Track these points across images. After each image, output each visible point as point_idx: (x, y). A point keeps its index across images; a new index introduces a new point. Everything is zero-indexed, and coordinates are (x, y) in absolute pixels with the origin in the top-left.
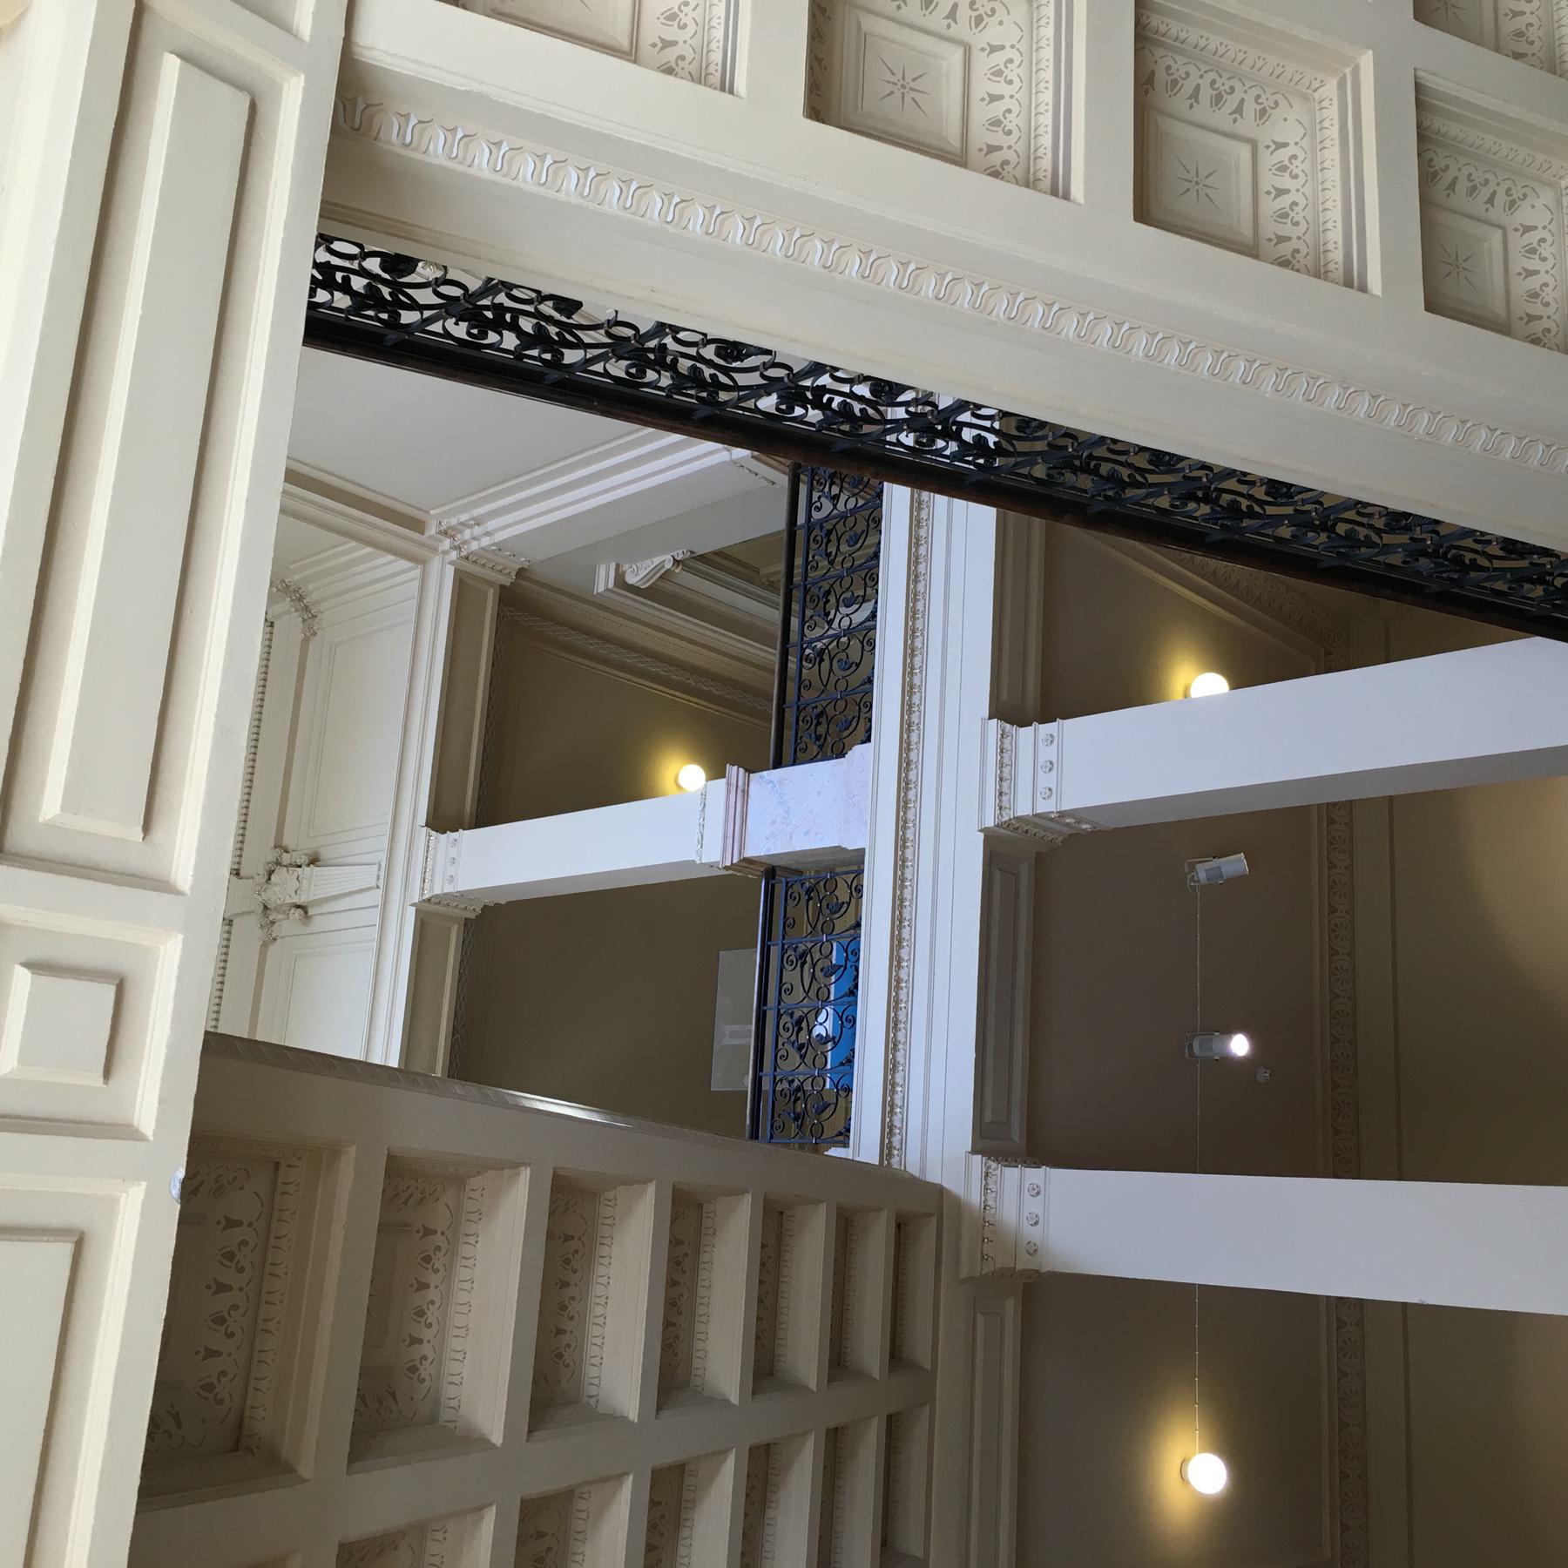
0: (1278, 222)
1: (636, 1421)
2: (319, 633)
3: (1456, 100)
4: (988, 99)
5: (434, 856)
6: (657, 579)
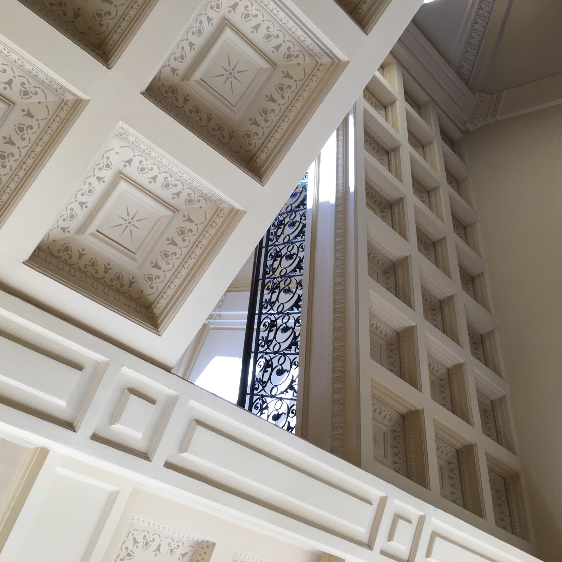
0: (146, 280)
3: (399, 154)
4: (255, 30)
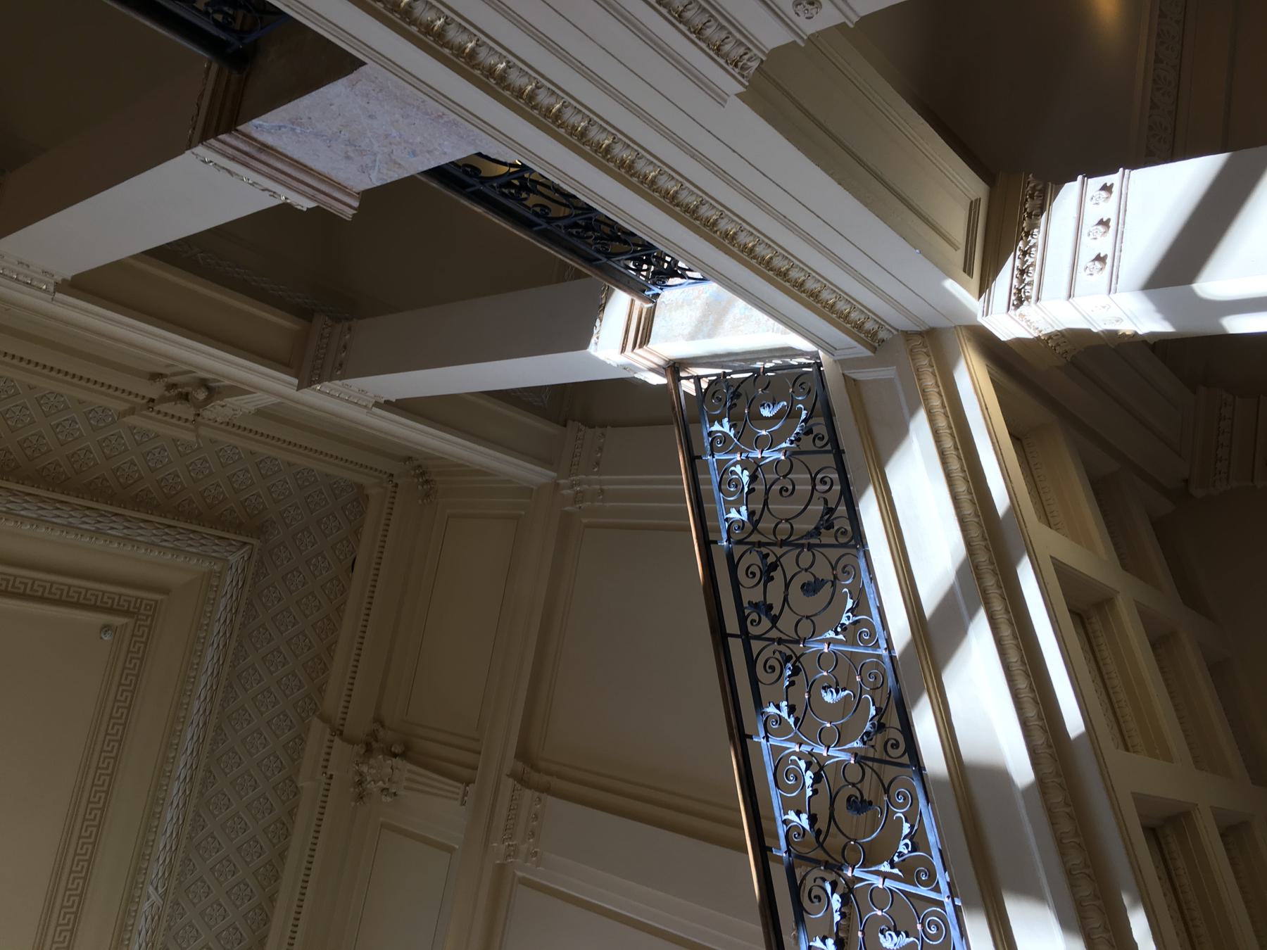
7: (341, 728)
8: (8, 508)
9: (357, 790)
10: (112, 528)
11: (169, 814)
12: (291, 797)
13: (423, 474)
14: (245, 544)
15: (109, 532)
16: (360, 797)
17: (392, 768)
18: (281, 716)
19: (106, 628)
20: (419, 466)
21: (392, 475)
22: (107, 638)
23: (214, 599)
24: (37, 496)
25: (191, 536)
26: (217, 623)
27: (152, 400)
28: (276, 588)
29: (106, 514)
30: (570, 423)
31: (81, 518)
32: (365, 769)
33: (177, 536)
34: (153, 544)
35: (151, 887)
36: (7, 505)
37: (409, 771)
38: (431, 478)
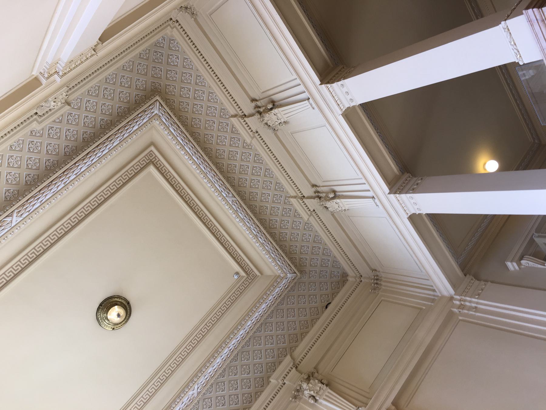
1: (506, 262)
2: (198, 14)
5: (335, 93)
6: (372, 397)
7: (297, 365)
8: (237, 210)
9: (296, 393)
10: (261, 238)
11: (219, 360)
12: (260, 387)
13: (377, 279)
14: (295, 273)
15: (259, 238)
16: (295, 397)
17: (320, 388)
18: (272, 350)
19: (237, 273)
20: (377, 276)
21: (361, 276)
22: (236, 277)
23: (275, 286)
24: (247, 212)
25: (281, 258)
26: (272, 296)
27: (304, 197)
28: (294, 298)
29: (262, 232)
30: (468, 276)
31: (254, 228)
32: (305, 386)
33: (277, 255)
34: (269, 252)
35: (197, 386)
36: (237, 209)
37: (328, 392)
38: (380, 283)
